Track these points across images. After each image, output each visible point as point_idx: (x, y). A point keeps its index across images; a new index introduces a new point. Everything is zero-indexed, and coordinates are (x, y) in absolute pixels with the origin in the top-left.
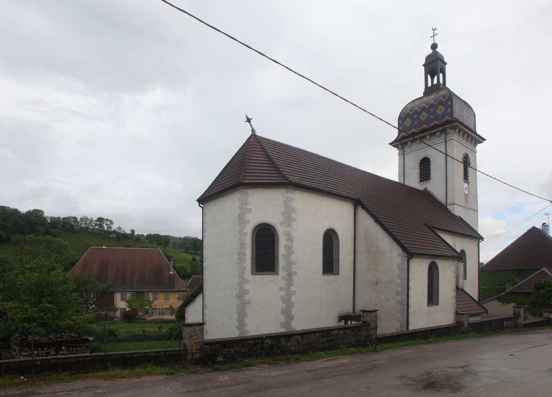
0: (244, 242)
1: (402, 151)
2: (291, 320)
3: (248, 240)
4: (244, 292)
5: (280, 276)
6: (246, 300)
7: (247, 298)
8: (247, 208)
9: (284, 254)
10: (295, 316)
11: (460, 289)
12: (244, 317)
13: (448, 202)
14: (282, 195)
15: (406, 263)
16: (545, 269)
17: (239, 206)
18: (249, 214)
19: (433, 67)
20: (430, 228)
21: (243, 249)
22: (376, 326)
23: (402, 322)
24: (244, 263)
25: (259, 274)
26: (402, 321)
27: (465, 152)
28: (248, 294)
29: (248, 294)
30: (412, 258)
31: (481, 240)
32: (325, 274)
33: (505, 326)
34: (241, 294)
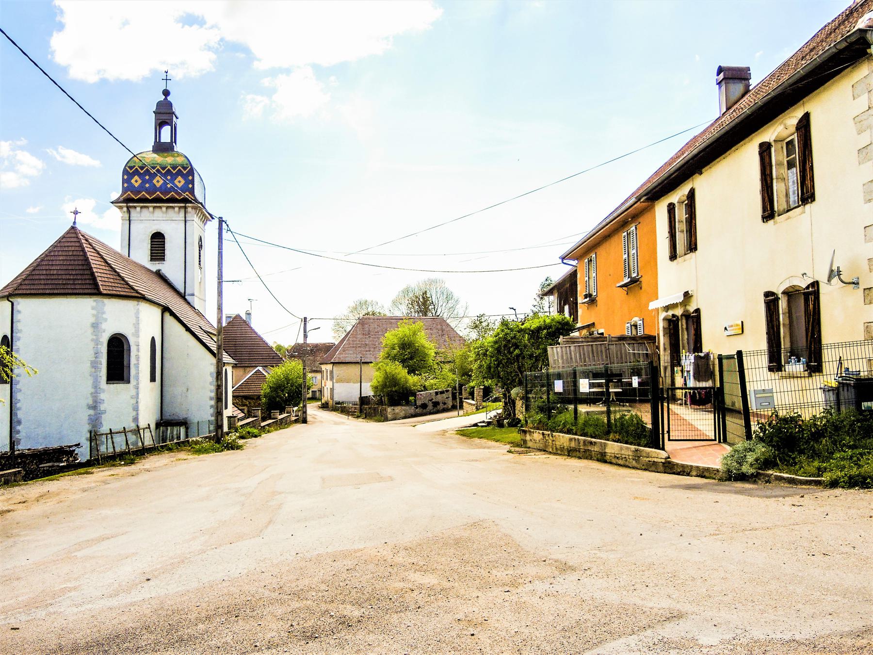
1: (127, 215)
16: (260, 369)
17: (134, 324)
19: (167, 119)
20: (205, 332)
24: (100, 372)
25: (113, 384)
32: (110, 382)
34: (94, 406)
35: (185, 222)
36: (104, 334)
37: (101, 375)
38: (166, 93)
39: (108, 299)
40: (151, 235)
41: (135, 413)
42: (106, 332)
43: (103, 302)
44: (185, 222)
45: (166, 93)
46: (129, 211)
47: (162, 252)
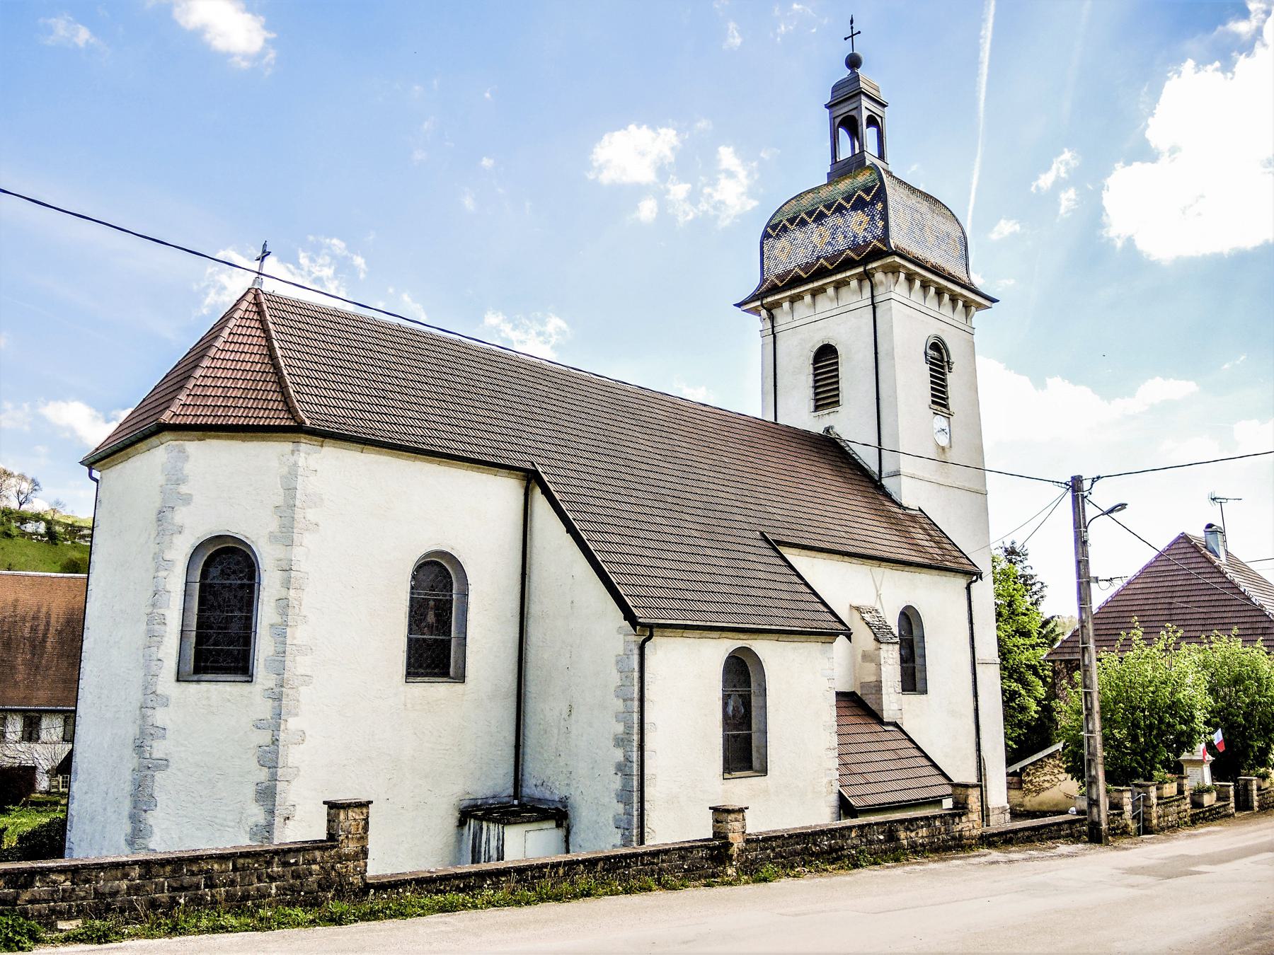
0: (165, 586)
2: (282, 820)
3: (175, 582)
4: (152, 732)
5: (257, 686)
6: (155, 755)
7: (158, 749)
8: (179, 493)
9: (272, 622)
10: (297, 807)
11: (889, 724)
12: (145, 808)
13: (883, 469)
14: (279, 459)
15: (636, 651)
18: (184, 509)
21: (160, 608)
22: (364, 852)
23: (627, 829)
26: (626, 826)
27: (933, 332)
28: (164, 737)
29: (164, 737)
30: (650, 638)
31: (975, 578)
33: (905, 842)
35: (874, 308)
36: (178, 540)
37: (160, 656)
38: (853, 62)
39: (196, 442)
40: (812, 354)
41: (263, 775)
42: (186, 532)
43: (183, 451)
44: (874, 308)
45: (853, 62)
46: (772, 314)
47: (820, 383)
